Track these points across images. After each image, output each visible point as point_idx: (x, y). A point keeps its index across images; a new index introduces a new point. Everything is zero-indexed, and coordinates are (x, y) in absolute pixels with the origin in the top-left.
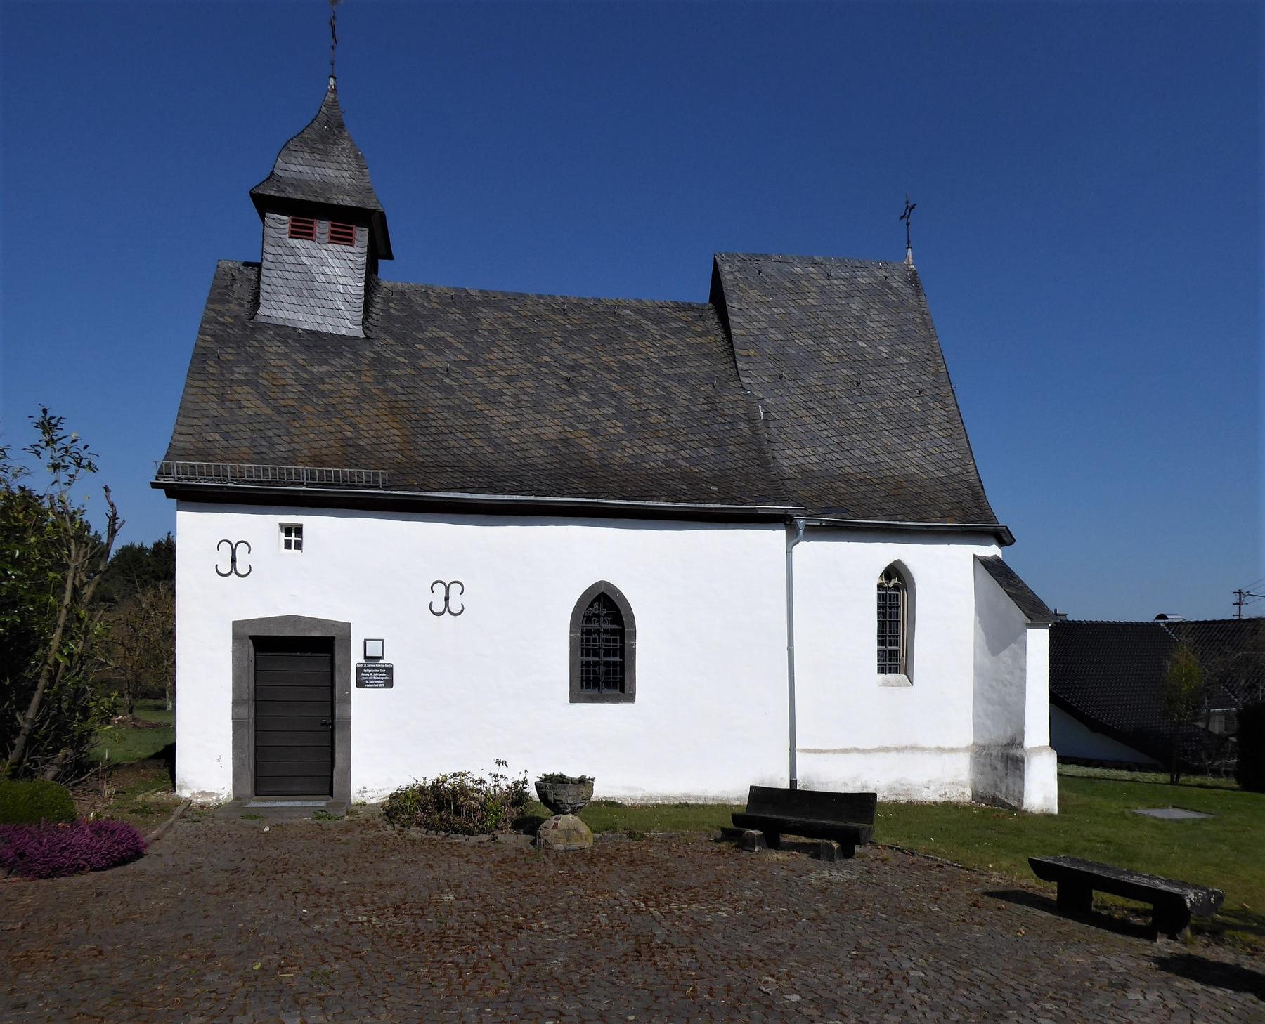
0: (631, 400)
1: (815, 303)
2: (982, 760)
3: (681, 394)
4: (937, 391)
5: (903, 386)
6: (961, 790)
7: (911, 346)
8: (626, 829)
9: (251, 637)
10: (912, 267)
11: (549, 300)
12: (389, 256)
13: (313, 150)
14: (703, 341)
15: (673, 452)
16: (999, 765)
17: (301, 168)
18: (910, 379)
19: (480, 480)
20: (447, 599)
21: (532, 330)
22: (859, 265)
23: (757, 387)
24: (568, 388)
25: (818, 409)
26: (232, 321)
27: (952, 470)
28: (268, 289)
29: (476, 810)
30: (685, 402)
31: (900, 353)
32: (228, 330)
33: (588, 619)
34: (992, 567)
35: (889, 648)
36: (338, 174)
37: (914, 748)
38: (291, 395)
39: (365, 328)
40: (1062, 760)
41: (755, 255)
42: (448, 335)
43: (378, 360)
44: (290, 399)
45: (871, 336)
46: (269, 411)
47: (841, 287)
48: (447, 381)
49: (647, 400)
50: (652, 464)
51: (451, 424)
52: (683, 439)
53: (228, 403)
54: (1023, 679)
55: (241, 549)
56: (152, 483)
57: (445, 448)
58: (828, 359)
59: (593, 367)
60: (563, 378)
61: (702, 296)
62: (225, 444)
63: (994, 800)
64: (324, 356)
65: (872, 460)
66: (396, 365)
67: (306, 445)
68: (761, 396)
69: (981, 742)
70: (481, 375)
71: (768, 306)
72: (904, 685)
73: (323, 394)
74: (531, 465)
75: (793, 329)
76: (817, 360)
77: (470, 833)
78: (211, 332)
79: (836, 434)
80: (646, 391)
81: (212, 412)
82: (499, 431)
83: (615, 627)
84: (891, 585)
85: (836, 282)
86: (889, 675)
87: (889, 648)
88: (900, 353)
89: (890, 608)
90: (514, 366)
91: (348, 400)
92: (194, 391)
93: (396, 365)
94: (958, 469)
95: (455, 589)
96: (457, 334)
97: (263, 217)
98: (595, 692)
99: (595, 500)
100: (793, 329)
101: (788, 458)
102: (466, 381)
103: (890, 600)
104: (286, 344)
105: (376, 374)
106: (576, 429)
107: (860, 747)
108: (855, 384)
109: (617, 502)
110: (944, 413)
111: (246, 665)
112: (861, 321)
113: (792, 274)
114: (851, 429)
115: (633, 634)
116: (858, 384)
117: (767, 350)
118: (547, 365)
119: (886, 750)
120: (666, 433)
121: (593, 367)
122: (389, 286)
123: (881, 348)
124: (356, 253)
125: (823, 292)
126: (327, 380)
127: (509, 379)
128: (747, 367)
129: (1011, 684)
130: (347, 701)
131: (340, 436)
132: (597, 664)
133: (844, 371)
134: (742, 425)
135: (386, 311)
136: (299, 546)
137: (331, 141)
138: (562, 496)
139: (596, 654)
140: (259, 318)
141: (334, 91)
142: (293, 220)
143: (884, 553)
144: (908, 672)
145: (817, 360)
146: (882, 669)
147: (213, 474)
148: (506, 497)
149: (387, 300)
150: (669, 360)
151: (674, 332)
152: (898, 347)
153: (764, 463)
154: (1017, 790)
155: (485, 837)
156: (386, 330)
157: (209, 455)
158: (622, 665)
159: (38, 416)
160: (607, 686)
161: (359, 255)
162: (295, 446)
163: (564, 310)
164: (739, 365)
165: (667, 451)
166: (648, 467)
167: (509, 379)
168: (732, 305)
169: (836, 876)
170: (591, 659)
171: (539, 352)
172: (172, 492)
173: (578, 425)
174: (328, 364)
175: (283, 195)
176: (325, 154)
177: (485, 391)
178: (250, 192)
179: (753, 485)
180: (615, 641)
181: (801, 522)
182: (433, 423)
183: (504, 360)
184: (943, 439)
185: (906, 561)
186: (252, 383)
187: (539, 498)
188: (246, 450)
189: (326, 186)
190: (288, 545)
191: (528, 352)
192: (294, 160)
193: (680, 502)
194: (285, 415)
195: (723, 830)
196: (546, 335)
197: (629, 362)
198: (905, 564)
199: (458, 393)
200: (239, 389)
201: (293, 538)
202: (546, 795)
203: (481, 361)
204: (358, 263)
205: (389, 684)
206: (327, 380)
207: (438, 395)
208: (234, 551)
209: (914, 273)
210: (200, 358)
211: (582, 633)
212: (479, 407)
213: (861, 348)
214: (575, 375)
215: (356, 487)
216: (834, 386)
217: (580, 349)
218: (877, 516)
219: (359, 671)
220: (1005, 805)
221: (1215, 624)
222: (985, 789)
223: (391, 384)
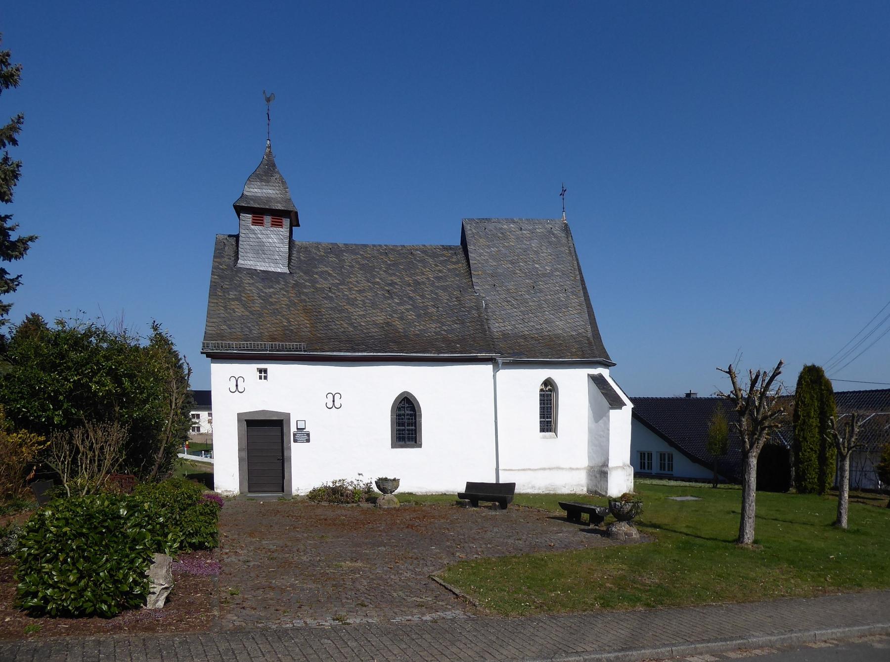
0: (419, 300)
1: (513, 244)
2: (591, 473)
3: (444, 296)
4: (575, 289)
5: (557, 287)
6: (581, 488)
7: (562, 266)
8: (415, 501)
9: (246, 420)
10: (565, 221)
11: (379, 248)
12: (298, 225)
13: (261, 180)
14: (456, 267)
15: (439, 327)
16: (598, 476)
17: (256, 190)
18: (561, 283)
19: (348, 345)
20: (334, 401)
21: (370, 265)
22: (538, 222)
23: (482, 291)
24: (388, 296)
25: (513, 302)
26: (226, 267)
27: (579, 331)
28: (242, 250)
29: (350, 494)
30: (446, 301)
31: (557, 270)
32: (225, 272)
33: (399, 409)
34: (599, 381)
35: (547, 420)
36: (274, 192)
37: (559, 468)
38: (257, 305)
39: (289, 268)
40: (637, 475)
41: (483, 219)
42: (329, 270)
43: (296, 285)
44: (257, 307)
45: (542, 261)
46: (248, 313)
47: (528, 235)
48: (330, 294)
49: (427, 300)
50: (429, 334)
51: (333, 317)
52: (444, 320)
53: (229, 310)
54: (608, 434)
55: (240, 380)
56: (201, 352)
57: (331, 329)
58: (519, 275)
59: (401, 284)
60: (386, 290)
61: (458, 242)
62: (229, 330)
63: (596, 492)
64: (271, 284)
65: (539, 327)
66: (305, 287)
67: (266, 330)
68: (484, 296)
69: (591, 465)
70: (346, 290)
71: (489, 247)
72: (554, 438)
73: (272, 304)
74: (371, 336)
75: (501, 259)
76: (513, 275)
77: (348, 503)
78: (217, 274)
79: (521, 314)
80: (427, 296)
81: (222, 315)
82: (356, 319)
83: (412, 412)
84: (547, 389)
85: (525, 232)
86: (546, 433)
87: (547, 420)
88: (557, 270)
89: (547, 400)
90: (362, 285)
91: (283, 306)
92: (213, 305)
93: (305, 287)
94: (583, 330)
95: (337, 397)
96: (334, 269)
97: (239, 216)
98: (402, 443)
99: (401, 354)
100: (501, 259)
101: (496, 327)
102: (339, 294)
103: (547, 396)
104: (252, 278)
105: (296, 292)
106: (393, 317)
107: (532, 468)
108: (532, 287)
109: (412, 355)
110: (577, 301)
111: (244, 433)
112: (537, 253)
113: (501, 229)
114: (529, 311)
115: (241, 460)
116: (534, 288)
117: (487, 271)
118: (378, 283)
119: (544, 469)
120: (436, 318)
121: (401, 284)
122: (300, 245)
123: (546, 267)
124: (284, 231)
125: (518, 238)
126: (273, 296)
127: (360, 292)
128: (477, 281)
129: (603, 437)
130: (290, 448)
131: (281, 325)
132: (404, 430)
133: (527, 281)
134: (474, 312)
135: (299, 258)
136: (266, 378)
137: (270, 174)
138: (386, 352)
139: (403, 425)
140: (239, 265)
141: (270, 147)
142: (254, 217)
143: (536, 376)
144: (555, 431)
145: (513, 275)
146: (542, 430)
147: (227, 346)
148: (360, 354)
149: (299, 252)
150: (438, 278)
151: (442, 262)
152: (555, 266)
153: (484, 331)
154: (605, 487)
155: (355, 505)
156: (299, 268)
157: (224, 336)
158: (415, 430)
159: (151, 324)
160: (409, 440)
161: (285, 232)
162: (262, 331)
163: (386, 253)
164: (473, 280)
165: (436, 327)
166: (427, 335)
167: (360, 292)
168: (470, 248)
169: (494, 513)
170: (401, 428)
171: (374, 277)
172: (208, 355)
173: (393, 315)
174: (273, 288)
175: (249, 206)
176: (268, 182)
177: (348, 299)
178: (234, 206)
179: (477, 343)
180: (412, 419)
181: (500, 360)
182: (324, 317)
183: (357, 281)
184: (576, 315)
185: (553, 378)
186: (238, 299)
187: (375, 354)
188: (239, 334)
189: (269, 199)
190: (260, 378)
191: (369, 277)
192: (253, 186)
193: (442, 353)
194: (255, 315)
195: (457, 501)
196: (378, 267)
197: (418, 280)
198: (553, 379)
199: (336, 301)
200: (233, 303)
201: (263, 375)
202: (379, 486)
203: (346, 282)
204: (285, 236)
205: (308, 441)
206: (273, 296)
207: (326, 302)
208: (237, 381)
209: (566, 225)
210: (214, 287)
211: (396, 416)
212: (346, 307)
213: (536, 268)
214: (392, 288)
215: (291, 351)
216: (521, 289)
217: (394, 274)
218: (538, 356)
219: (295, 435)
220: (600, 495)
221: (854, 393)
222: (592, 487)
223: (303, 297)
